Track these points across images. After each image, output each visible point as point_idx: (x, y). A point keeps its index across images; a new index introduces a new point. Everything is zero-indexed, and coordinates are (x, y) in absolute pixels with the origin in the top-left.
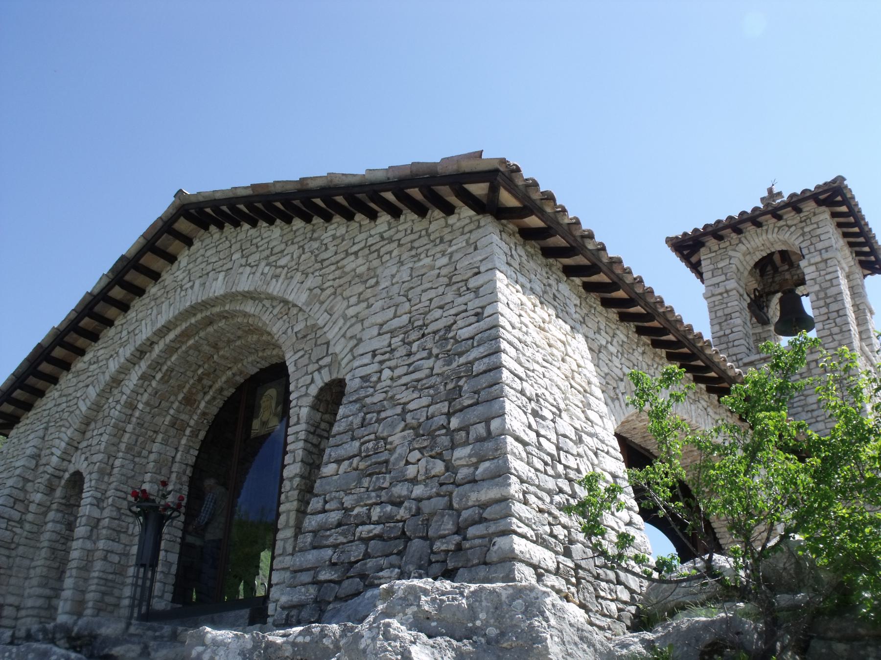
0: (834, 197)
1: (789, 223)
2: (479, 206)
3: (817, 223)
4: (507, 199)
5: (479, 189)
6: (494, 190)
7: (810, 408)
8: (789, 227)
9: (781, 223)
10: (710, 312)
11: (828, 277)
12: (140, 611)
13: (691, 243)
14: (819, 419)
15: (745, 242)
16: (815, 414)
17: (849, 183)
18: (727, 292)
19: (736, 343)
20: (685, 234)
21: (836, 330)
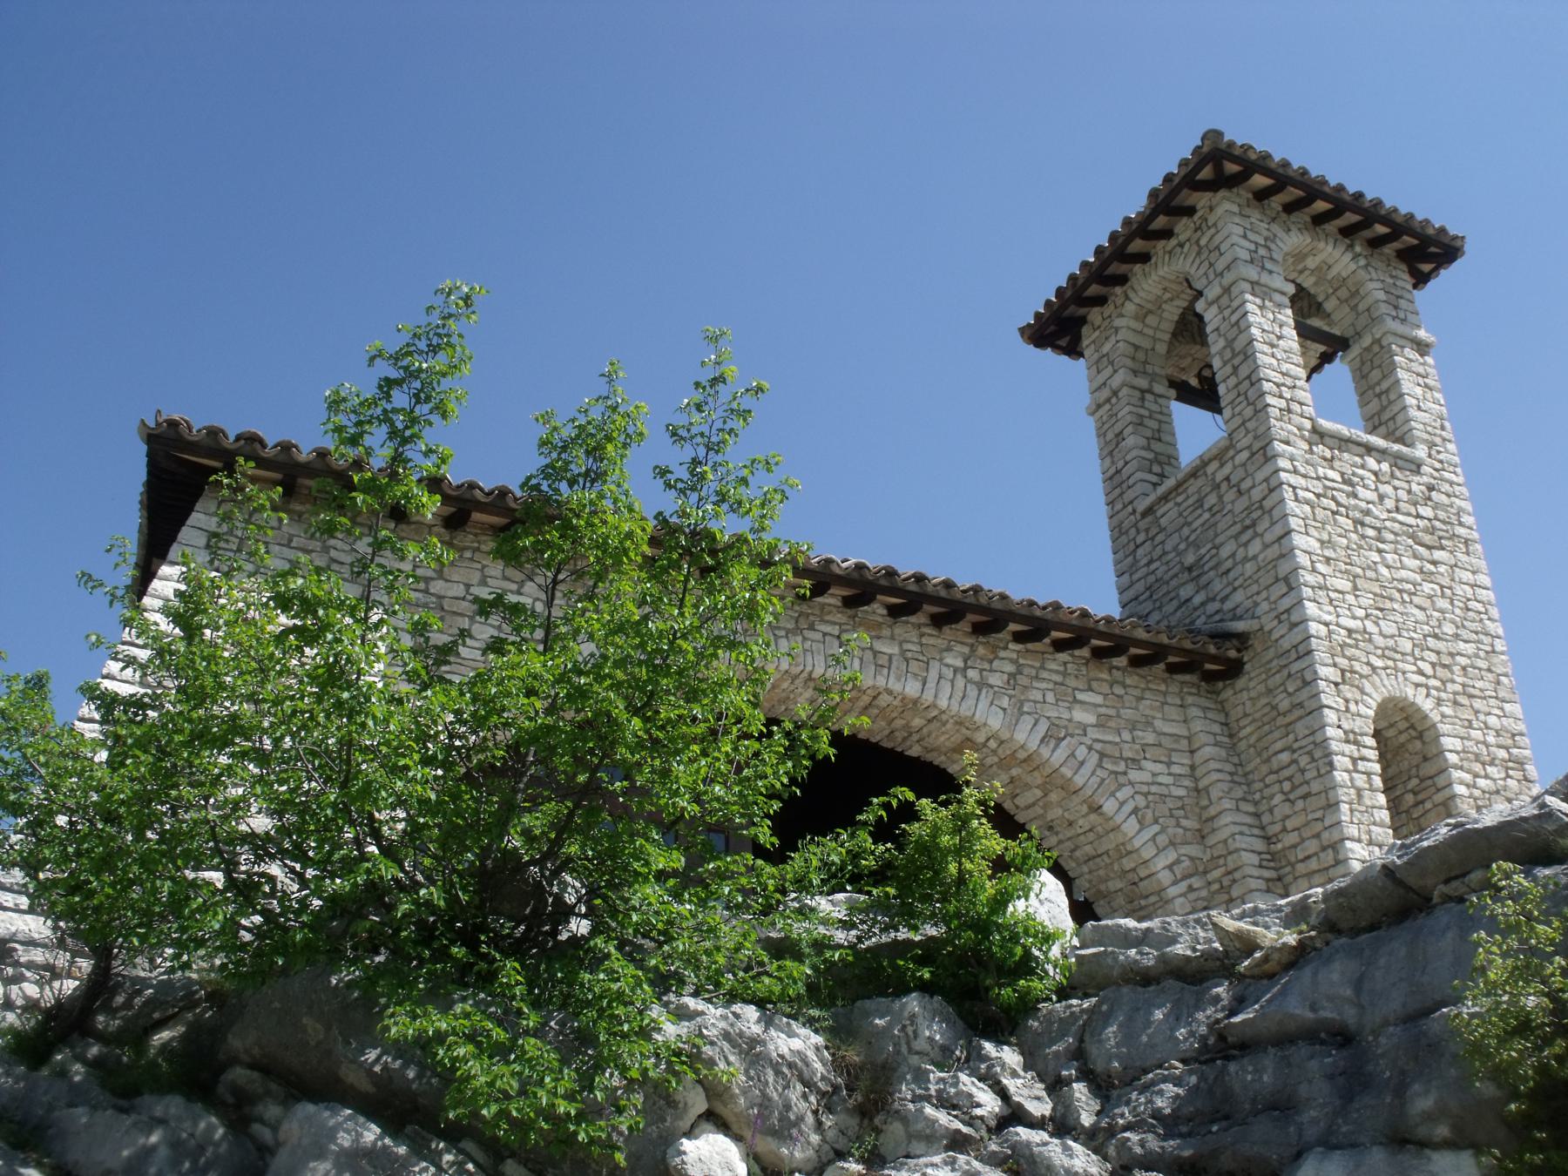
0: (1219, 169)
1: (1182, 238)
2: (1212, 186)
3: (1215, 225)
4: (1231, 168)
5: (1206, 173)
6: (1218, 169)
7: (1223, 568)
8: (1181, 245)
9: (1173, 242)
10: (1099, 436)
11: (1234, 318)
12: (1270, 367)
13: (1052, 328)
14: (1237, 584)
15: (1132, 295)
16: (1232, 575)
17: (1237, 134)
18: (1115, 393)
19: (1131, 481)
20: (1038, 316)
21: (1249, 412)
